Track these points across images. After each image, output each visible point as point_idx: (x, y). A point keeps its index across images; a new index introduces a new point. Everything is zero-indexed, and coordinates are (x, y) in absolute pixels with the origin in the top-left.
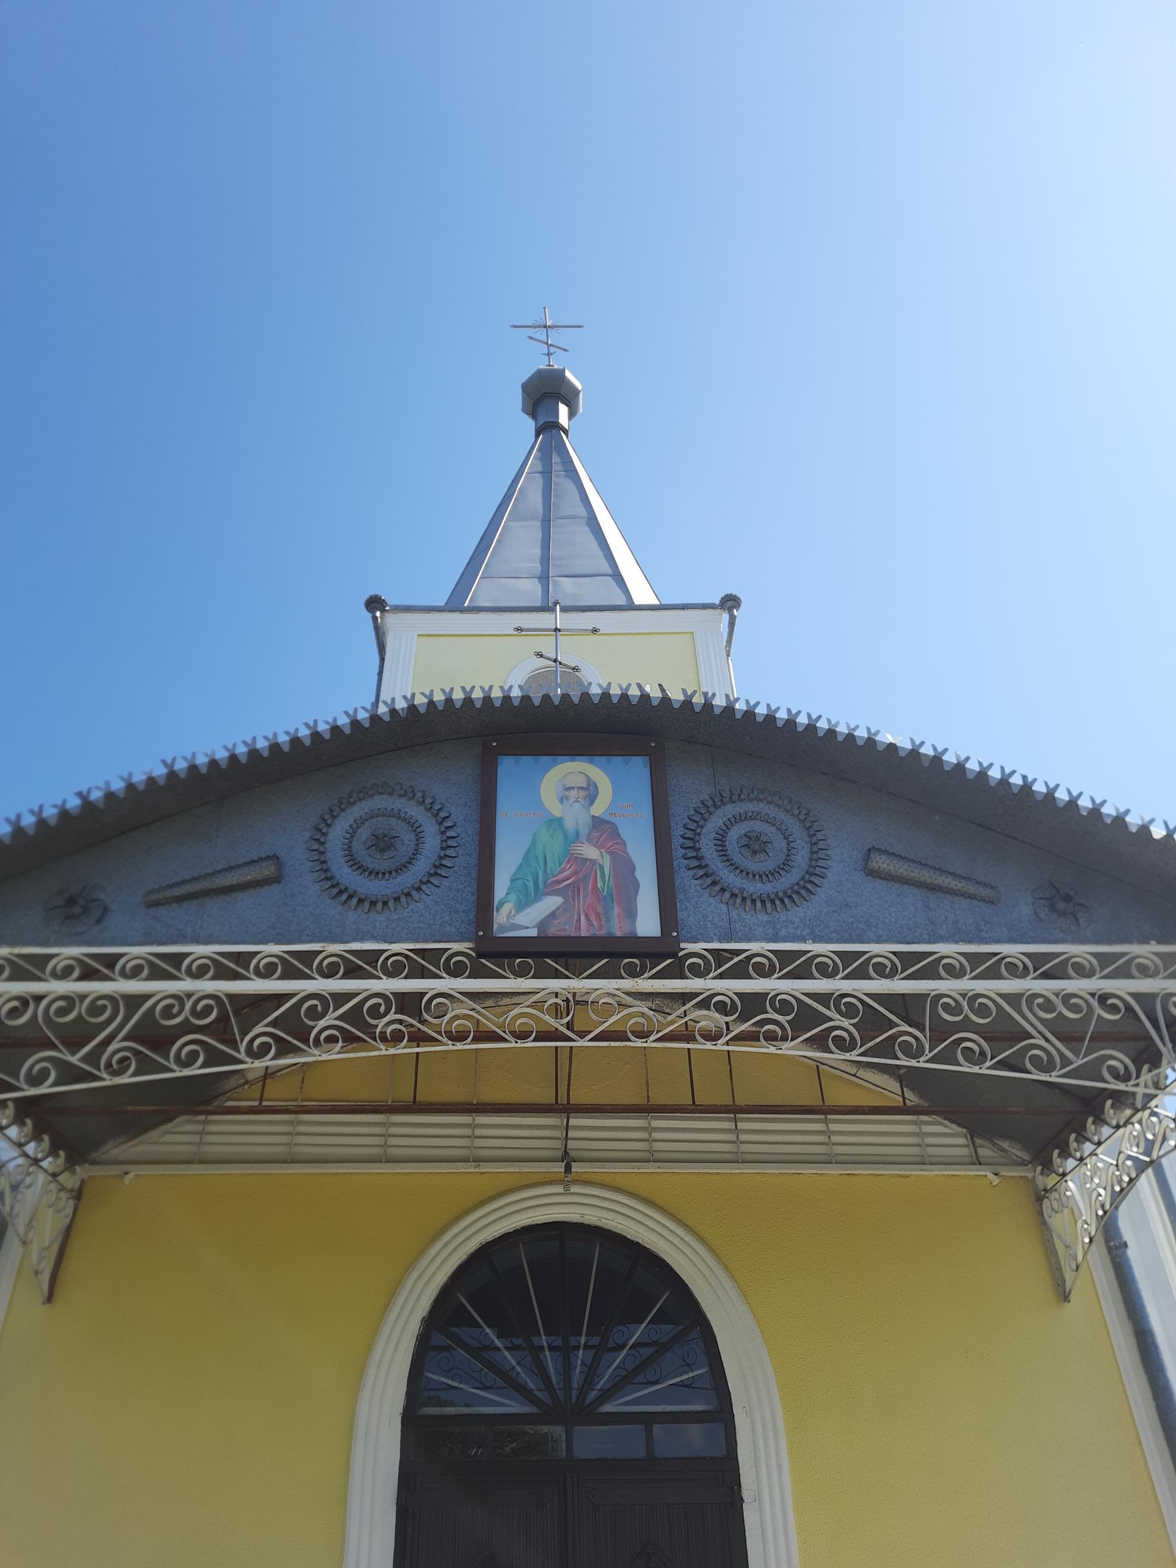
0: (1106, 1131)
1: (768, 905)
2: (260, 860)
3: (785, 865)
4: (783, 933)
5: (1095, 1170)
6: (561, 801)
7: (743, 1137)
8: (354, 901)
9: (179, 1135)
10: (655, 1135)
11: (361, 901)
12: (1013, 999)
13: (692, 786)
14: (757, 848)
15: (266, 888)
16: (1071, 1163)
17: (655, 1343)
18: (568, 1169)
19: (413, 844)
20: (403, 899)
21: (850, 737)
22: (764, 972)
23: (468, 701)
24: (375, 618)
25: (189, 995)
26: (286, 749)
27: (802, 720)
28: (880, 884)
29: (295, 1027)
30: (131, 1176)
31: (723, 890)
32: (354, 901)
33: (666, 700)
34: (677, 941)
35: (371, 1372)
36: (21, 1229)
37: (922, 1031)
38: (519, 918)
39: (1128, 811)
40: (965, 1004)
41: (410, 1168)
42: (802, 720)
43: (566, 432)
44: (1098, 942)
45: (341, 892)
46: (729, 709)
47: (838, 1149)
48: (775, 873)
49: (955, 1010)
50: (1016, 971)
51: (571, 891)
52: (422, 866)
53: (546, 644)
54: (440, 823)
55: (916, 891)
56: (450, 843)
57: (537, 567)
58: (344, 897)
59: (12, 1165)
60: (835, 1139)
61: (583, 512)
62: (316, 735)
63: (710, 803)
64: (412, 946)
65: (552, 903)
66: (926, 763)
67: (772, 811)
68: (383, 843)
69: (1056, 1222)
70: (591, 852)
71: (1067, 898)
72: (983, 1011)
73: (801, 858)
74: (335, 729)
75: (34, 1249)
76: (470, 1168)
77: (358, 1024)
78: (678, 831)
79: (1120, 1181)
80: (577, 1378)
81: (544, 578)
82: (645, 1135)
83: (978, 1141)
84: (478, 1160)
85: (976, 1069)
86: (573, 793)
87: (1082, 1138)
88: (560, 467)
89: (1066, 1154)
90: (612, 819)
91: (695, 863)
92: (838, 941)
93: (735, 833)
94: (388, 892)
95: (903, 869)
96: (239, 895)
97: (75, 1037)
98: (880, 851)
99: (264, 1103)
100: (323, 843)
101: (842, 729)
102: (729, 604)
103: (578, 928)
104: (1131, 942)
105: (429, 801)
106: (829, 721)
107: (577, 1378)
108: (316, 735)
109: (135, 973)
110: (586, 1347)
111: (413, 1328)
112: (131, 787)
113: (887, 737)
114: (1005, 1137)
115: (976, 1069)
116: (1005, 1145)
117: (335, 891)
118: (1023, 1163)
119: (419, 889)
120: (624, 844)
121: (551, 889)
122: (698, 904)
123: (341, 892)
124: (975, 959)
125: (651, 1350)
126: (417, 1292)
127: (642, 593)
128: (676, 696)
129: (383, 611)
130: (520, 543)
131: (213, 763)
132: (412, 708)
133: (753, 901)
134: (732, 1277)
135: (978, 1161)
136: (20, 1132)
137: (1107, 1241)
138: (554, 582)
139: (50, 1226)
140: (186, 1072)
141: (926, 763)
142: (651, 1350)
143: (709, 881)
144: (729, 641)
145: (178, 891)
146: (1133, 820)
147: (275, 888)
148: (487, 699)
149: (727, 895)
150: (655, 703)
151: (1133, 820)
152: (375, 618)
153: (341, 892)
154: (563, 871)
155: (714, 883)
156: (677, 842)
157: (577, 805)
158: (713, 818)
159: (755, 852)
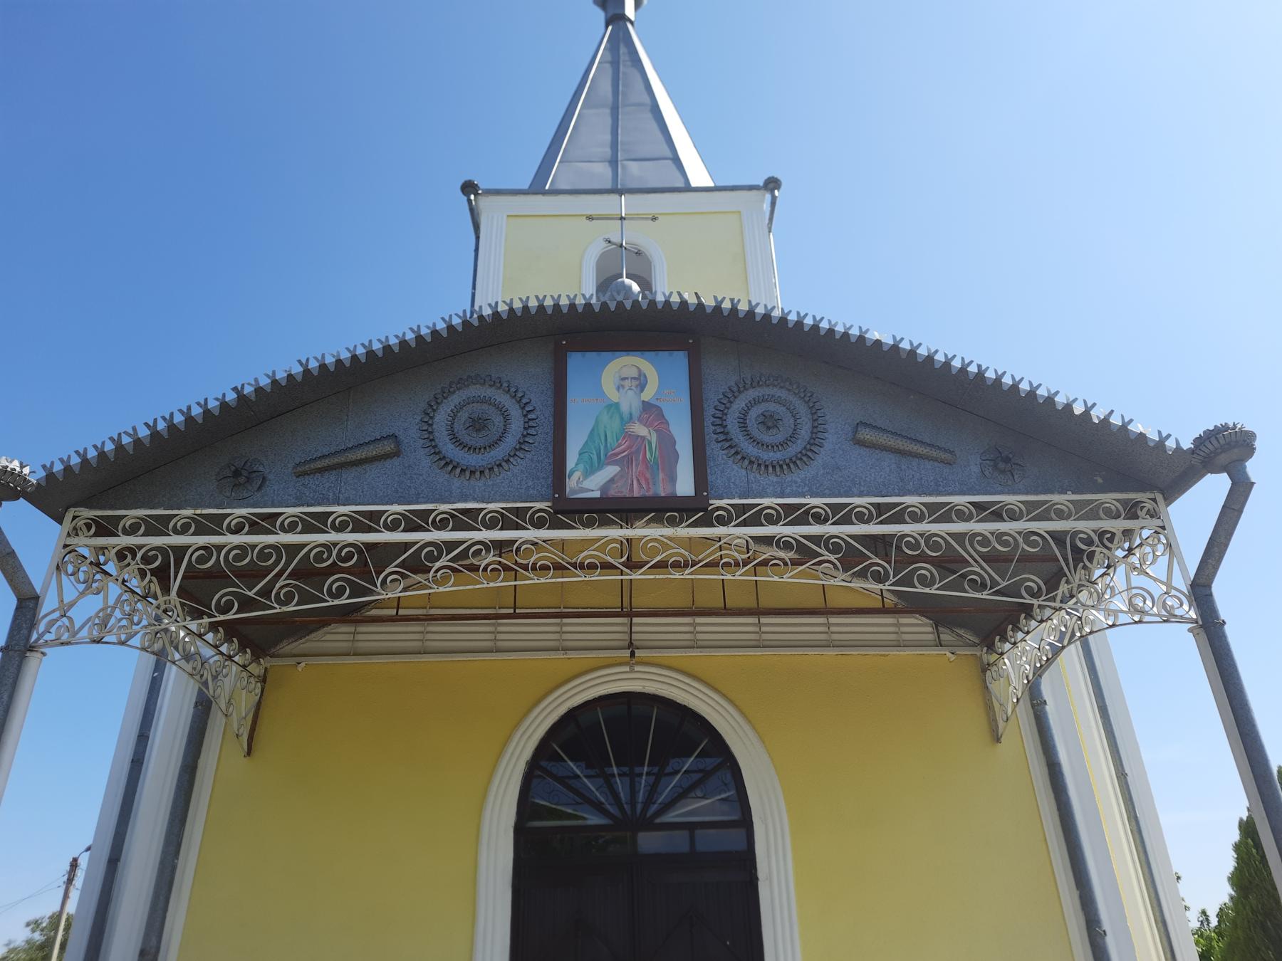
0: (1033, 623)
1: (778, 469)
2: (382, 438)
3: (792, 437)
4: (788, 491)
5: (1024, 652)
6: (618, 389)
7: (763, 629)
8: (458, 470)
9: (337, 636)
10: (699, 629)
11: (463, 470)
12: (959, 537)
13: (720, 376)
14: (770, 424)
15: (388, 463)
16: (1007, 646)
17: (700, 771)
18: (633, 654)
19: (501, 425)
20: (496, 469)
21: (846, 335)
22: (772, 521)
23: (541, 307)
24: (469, 201)
25: (335, 545)
26: (396, 350)
27: (808, 321)
28: (864, 451)
29: (417, 564)
30: (303, 665)
31: (743, 458)
32: (458, 470)
33: (700, 305)
34: (707, 498)
35: (491, 798)
36: (223, 707)
37: (889, 563)
38: (587, 483)
39: (1057, 393)
40: (922, 542)
41: (513, 656)
42: (808, 321)
43: (632, 23)
44: (1027, 494)
45: (448, 464)
46: (751, 313)
47: (835, 637)
48: (783, 444)
49: (916, 546)
50: (963, 516)
51: (626, 462)
52: (510, 441)
53: (612, 230)
54: (523, 408)
55: (892, 456)
56: (531, 423)
57: (607, 151)
58: (450, 467)
59: (211, 661)
60: (833, 629)
61: (647, 100)
62: (419, 338)
63: (735, 389)
64: (504, 505)
65: (611, 471)
66: (904, 356)
67: (783, 394)
68: (478, 424)
69: (994, 687)
70: (641, 430)
71: (1007, 460)
72: (935, 546)
73: (805, 432)
74: (435, 333)
75: (235, 717)
76: (560, 655)
77: (464, 561)
78: (709, 412)
79: (1040, 661)
80: (641, 797)
81: (614, 162)
82: (691, 629)
83: (941, 629)
84: (565, 649)
85: (927, 590)
86: (627, 383)
87: (1017, 628)
88: (627, 58)
89: (1004, 639)
90: (658, 403)
91: (722, 437)
92: (829, 496)
93: (754, 413)
94: (484, 463)
95: (883, 439)
96: (367, 466)
97: (251, 575)
98: (865, 425)
99: (401, 612)
100: (431, 425)
101: (840, 328)
102: (771, 185)
103: (631, 490)
104: (1052, 493)
105: (513, 390)
106: (830, 322)
107: (641, 797)
108: (419, 338)
109: (291, 528)
110: (648, 774)
111: (521, 767)
112: (275, 382)
113: (874, 335)
114: (961, 626)
115: (927, 590)
116: (961, 632)
117: (443, 463)
118: (974, 645)
119: (508, 461)
120: (667, 423)
121: (611, 460)
122: (725, 469)
123: (447, 464)
124: (932, 508)
125: (700, 775)
126: (522, 743)
127: (699, 175)
128: (709, 302)
129: (476, 194)
130: (592, 131)
131: (339, 362)
132: (496, 314)
133: (766, 466)
134: (754, 728)
135: (940, 644)
136: (215, 636)
137: (1031, 700)
138: (623, 167)
139: (245, 703)
140: (337, 602)
141: (904, 356)
142: (700, 775)
143: (733, 451)
144: (771, 219)
145: (319, 464)
146: (1061, 400)
147: (396, 461)
148: (557, 306)
149: (746, 462)
150: (691, 309)
151: (1061, 400)
152: (469, 201)
153: (448, 464)
154: (620, 445)
155: (737, 453)
156: (708, 420)
157: (630, 393)
158: (737, 401)
159: (769, 428)
